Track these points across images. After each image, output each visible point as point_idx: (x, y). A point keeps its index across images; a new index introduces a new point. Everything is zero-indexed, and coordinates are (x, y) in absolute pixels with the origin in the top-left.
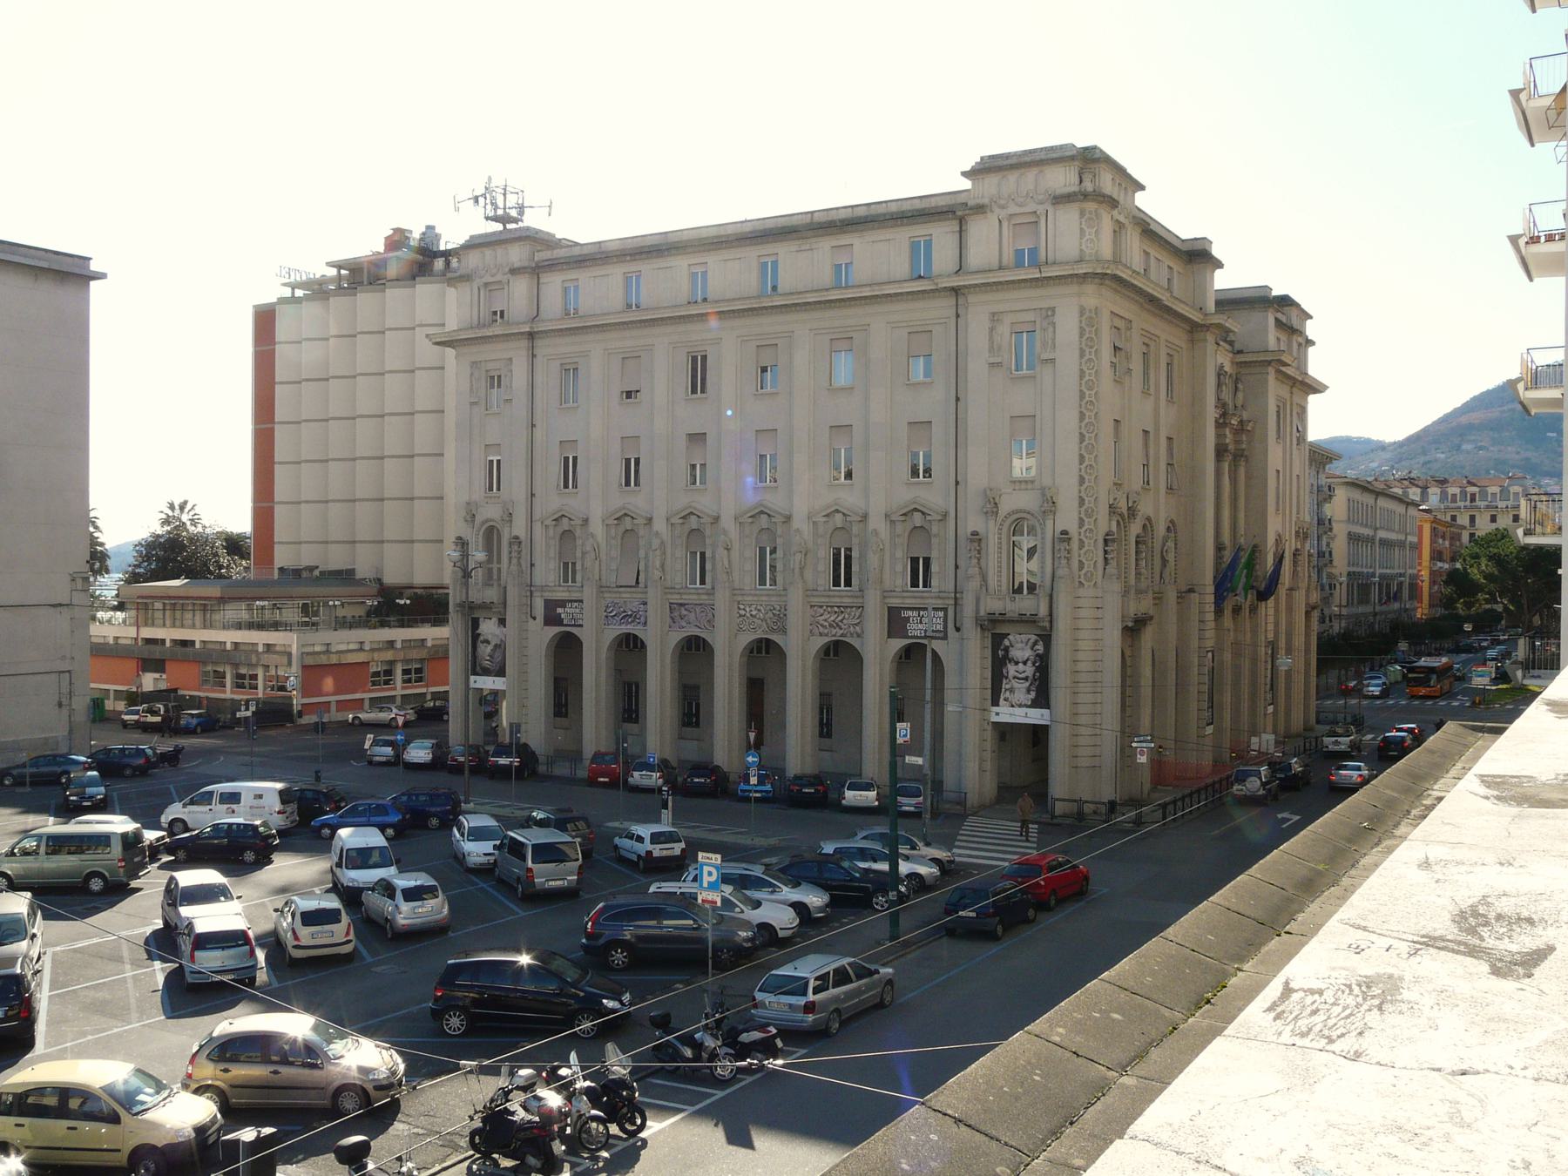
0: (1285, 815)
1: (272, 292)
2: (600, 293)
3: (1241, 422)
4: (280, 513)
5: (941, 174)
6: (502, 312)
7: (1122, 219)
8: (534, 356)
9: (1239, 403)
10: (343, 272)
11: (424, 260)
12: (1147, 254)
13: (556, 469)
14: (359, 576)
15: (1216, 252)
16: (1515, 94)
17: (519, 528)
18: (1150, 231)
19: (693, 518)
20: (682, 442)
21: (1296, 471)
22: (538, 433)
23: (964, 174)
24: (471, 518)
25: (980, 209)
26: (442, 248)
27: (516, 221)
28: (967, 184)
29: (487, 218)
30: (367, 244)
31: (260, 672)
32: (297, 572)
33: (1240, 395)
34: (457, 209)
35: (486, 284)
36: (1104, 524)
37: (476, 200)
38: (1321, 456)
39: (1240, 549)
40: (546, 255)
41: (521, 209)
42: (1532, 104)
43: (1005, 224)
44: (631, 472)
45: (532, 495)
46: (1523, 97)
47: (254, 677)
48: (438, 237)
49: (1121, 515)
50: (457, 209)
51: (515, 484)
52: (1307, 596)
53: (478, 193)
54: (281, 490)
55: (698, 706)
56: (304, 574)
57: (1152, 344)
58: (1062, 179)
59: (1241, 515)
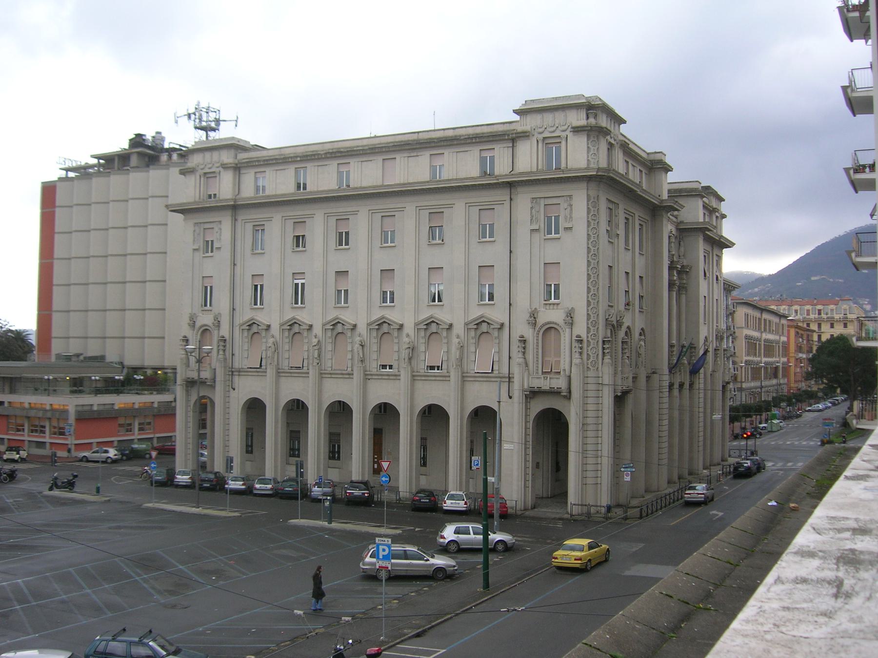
0: (714, 512)
1: (54, 174)
2: (280, 183)
3: (683, 266)
4: (56, 319)
5: (500, 113)
6: (215, 195)
7: (612, 141)
8: (236, 220)
9: (681, 254)
10: (102, 161)
11: (145, 153)
12: (627, 162)
13: (249, 293)
14: (109, 359)
15: (668, 160)
16: (844, 88)
17: (225, 331)
18: (626, 148)
19: (484, 325)
20: (332, 276)
21: (715, 297)
22: (238, 269)
23: (515, 112)
24: (193, 324)
25: (525, 135)
26: (166, 146)
27: (214, 130)
28: (517, 118)
29: (196, 128)
30: (119, 143)
31: (47, 424)
32: (68, 358)
33: (682, 249)
34: (176, 122)
35: (205, 173)
36: (602, 332)
37: (189, 116)
38: (729, 287)
39: (683, 346)
40: (243, 156)
41: (218, 121)
42: (855, 95)
43: (540, 145)
44: (299, 293)
45: (234, 309)
46: (849, 90)
47: (44, 427)
48: (163, 139)
49: (613, 326)
50: (176, 122)
51: (221, 302)
52: (723, 376)
53: (190, 112)
54: (58, 302)
55: (339, 447)
56: (74, 359)
57: (630, 218)
58: (578, 119)
59: (683, 325)
